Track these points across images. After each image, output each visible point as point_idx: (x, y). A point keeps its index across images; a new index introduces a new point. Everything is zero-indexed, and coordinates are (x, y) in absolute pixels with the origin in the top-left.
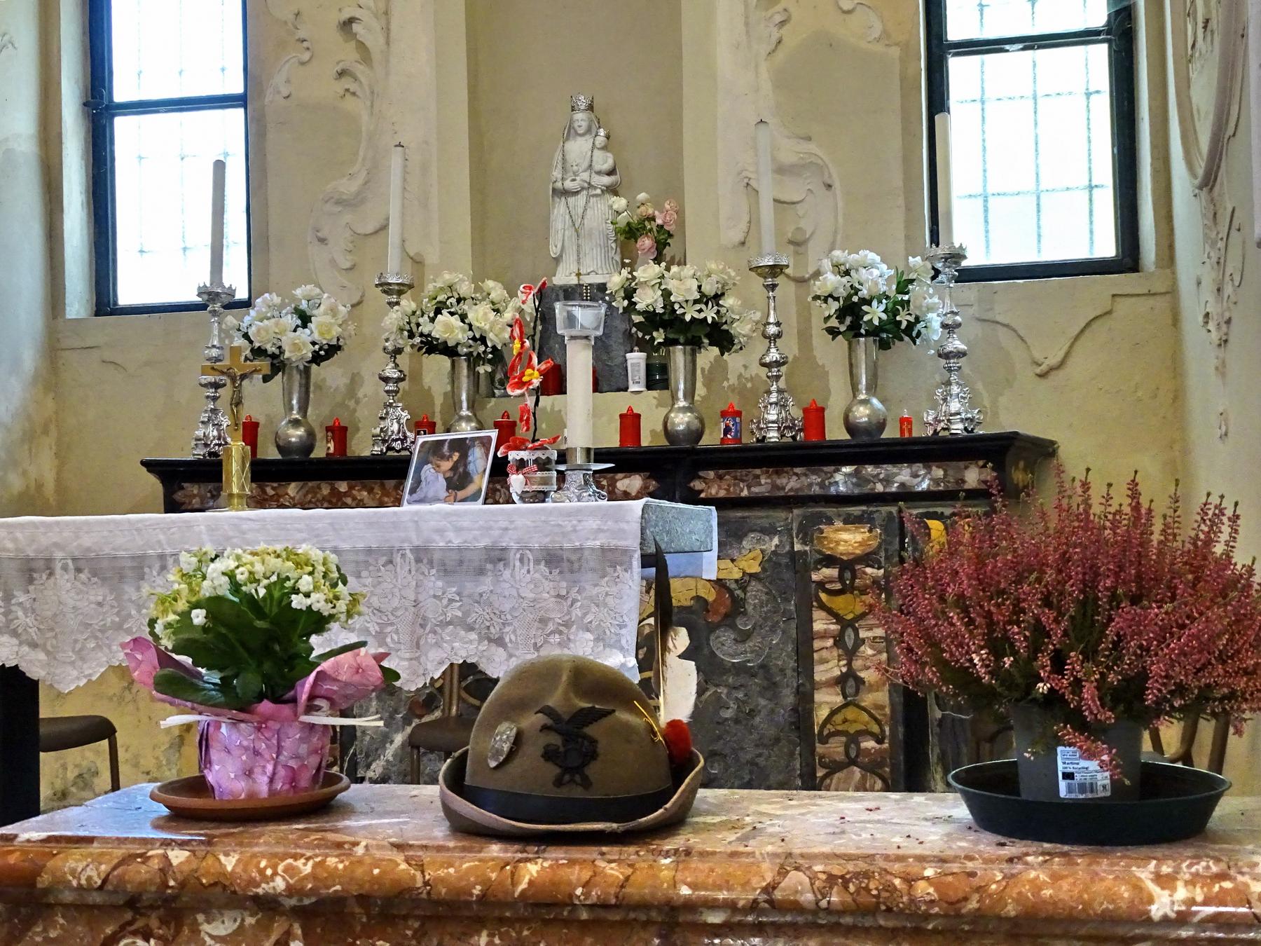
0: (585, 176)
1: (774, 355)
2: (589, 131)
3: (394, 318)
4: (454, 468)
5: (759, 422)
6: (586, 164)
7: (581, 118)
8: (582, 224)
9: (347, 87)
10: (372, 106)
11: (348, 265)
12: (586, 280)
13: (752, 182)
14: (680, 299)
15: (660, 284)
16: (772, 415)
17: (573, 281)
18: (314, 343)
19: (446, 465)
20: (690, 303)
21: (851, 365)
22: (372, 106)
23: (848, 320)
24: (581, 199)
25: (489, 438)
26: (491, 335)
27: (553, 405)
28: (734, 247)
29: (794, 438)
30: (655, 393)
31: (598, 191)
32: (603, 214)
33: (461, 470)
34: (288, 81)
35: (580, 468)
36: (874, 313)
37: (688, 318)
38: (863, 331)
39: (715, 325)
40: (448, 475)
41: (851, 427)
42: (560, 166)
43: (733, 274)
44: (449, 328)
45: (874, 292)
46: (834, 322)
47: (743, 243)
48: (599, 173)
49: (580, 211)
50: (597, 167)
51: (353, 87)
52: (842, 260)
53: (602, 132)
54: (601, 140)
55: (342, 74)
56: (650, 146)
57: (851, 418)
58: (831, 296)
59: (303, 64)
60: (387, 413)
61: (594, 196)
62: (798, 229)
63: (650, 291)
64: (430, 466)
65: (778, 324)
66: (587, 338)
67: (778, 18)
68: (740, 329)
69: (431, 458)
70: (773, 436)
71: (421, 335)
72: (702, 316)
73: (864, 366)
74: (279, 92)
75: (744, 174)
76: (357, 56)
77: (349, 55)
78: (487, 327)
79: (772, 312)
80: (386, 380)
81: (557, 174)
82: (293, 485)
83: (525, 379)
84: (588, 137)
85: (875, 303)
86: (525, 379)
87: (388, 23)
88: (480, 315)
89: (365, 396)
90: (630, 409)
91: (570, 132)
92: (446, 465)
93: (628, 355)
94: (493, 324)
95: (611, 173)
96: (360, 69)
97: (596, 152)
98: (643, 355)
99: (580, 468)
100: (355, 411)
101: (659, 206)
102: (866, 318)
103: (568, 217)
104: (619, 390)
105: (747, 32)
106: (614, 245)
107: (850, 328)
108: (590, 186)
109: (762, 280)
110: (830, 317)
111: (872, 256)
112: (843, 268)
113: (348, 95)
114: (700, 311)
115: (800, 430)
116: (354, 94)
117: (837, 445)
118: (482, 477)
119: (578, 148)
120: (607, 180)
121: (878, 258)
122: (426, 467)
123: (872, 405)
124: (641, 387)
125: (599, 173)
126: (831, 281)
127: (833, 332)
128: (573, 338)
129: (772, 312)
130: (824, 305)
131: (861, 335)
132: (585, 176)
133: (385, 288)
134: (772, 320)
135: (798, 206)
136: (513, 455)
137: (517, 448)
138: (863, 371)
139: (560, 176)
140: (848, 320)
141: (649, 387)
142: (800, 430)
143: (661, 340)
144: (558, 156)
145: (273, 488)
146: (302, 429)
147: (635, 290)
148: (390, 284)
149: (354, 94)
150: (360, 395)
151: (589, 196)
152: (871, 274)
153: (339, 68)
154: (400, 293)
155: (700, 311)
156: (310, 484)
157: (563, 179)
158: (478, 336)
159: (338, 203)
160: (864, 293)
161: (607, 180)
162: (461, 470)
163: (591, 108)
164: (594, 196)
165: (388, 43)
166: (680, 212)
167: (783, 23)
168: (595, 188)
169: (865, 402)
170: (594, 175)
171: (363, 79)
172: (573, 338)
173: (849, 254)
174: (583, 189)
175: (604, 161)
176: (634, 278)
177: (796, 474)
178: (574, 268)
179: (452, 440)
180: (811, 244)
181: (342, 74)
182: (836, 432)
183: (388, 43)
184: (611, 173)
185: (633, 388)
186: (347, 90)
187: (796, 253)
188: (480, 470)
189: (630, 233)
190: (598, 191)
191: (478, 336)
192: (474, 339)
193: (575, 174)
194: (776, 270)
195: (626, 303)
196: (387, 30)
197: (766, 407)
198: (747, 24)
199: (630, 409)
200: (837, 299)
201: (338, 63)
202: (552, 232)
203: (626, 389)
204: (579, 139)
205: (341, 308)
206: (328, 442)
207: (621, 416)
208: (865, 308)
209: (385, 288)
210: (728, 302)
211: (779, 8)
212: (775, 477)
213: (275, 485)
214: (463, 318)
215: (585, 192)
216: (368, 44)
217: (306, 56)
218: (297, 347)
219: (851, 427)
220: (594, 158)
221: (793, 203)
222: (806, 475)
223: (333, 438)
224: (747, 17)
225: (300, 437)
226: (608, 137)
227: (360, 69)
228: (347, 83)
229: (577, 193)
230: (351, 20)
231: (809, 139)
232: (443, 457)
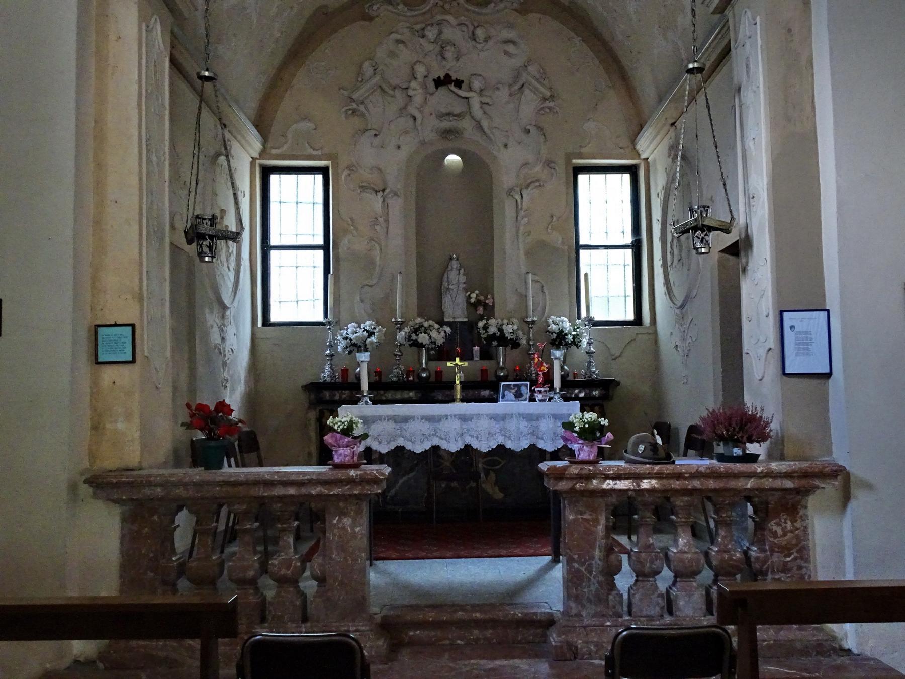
17: (452, 320)
80: (396, 355)
111: (565, 319)
124: (478, 359)
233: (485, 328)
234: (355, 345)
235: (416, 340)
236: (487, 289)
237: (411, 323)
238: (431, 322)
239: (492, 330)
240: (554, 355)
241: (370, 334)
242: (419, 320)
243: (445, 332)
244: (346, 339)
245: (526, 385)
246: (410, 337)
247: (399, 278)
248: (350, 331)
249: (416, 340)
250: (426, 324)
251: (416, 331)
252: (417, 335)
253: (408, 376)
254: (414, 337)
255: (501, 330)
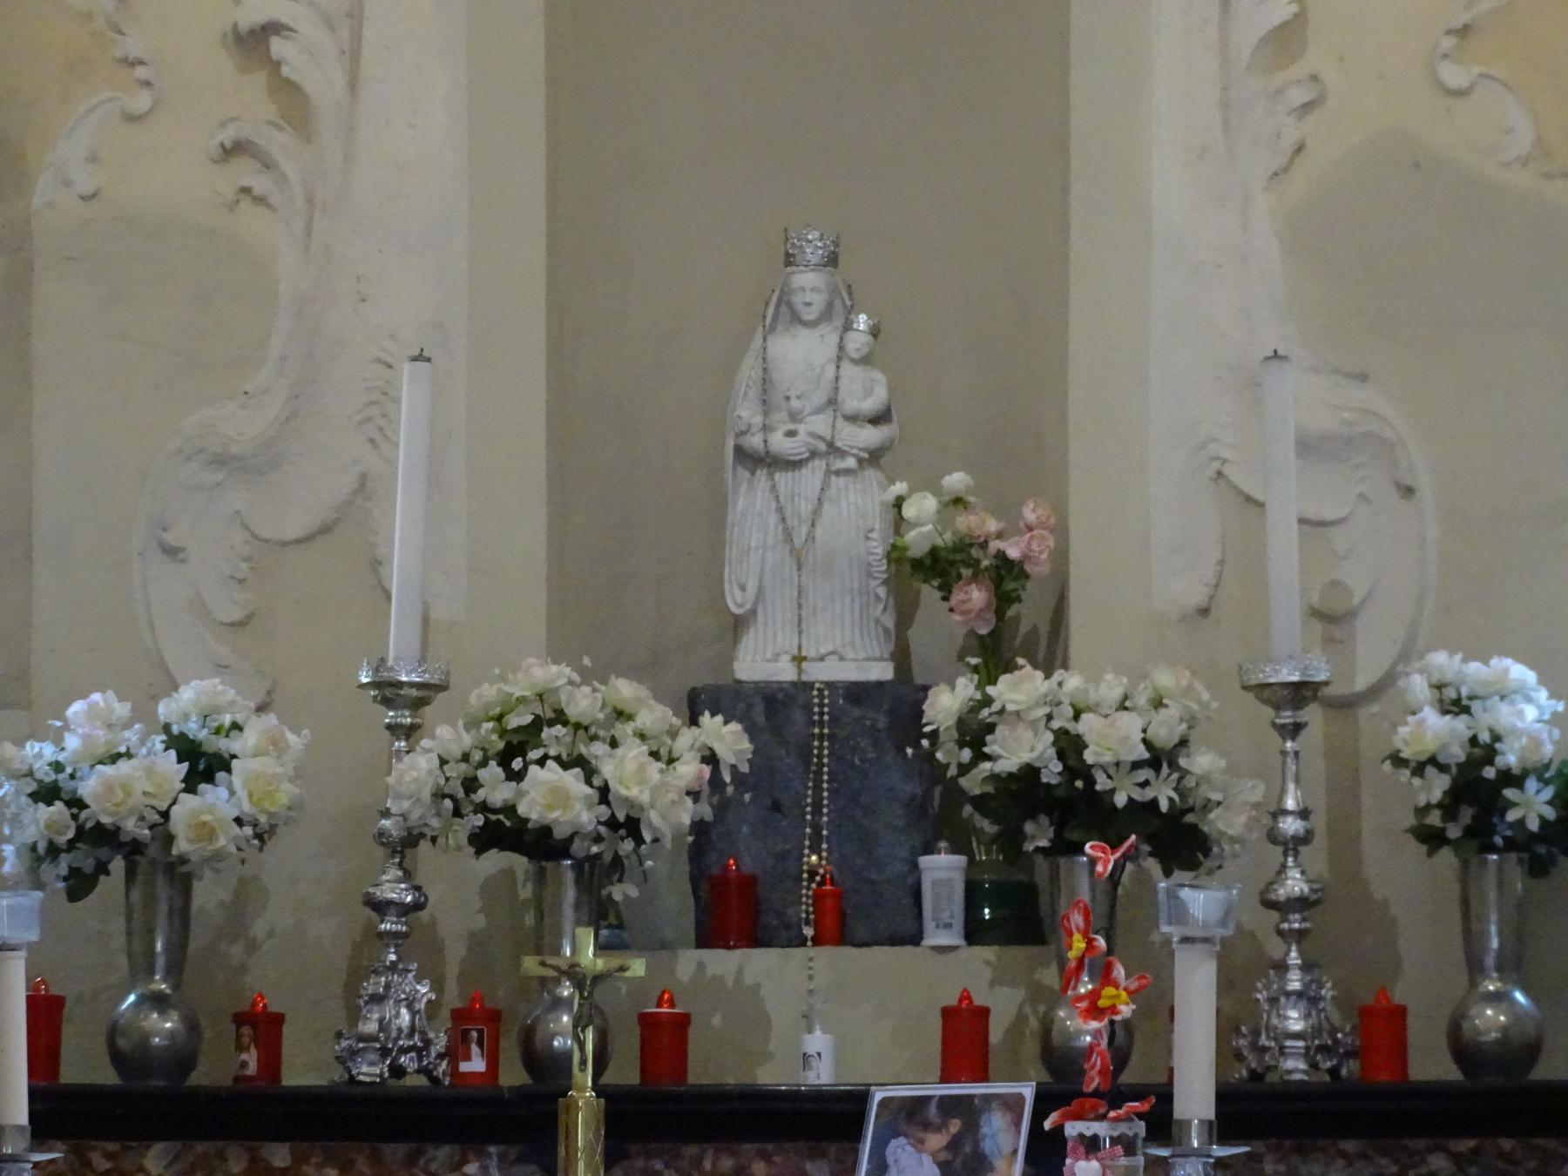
0: (821, 424)
1: (1295, 884)
2: (826, 315)
3: (417, 770)
4: (954, 1145)
5: (1256, 1033)
6: (820, 397)
7: (809, 284)
8: (811, 538)
9: (246, 182)
10: (309, 233)
11: (236, 614)
12: (819, 673)
13: (1226, 470)
14: (1108, 758)
15: (1049, 717)
16: (1295, 1020)
17: (785, 672)
18: (239, 821)
19: (937, 1141)
20: (1125, 768)
21: (1465, 903)
22: (309, 233)
23: (1467, 814)
24: (810, 478)
25: (1020, 1099)
26: (654, 817)
27: (740, 972)
28: (1183, 618)
29: (1334, 1072)
30: (988, 953)
31: (851, 462)
32: (853, 517)
33: (968, 1149)
34: (93, 158)
35: (1197, 1153)
36: (1528, 805)
37: (1120, 800)
38: (1498, 840)
39: (1177, 813)
40: (943, 1156)
41: (1462, 1049)
42: (753, 394)
43: (1205, 696)
44: (560, 797)
45: (1534, 759)
46: (1434, 819)
47: (1204, 612)
48: (852, 419)
49: (805, 508)
50: (851, 404)
51: (261, 184)
52: (1449, 676)
53: (862, 321)
54: (858, 340)
55: (235, 150)
56: (993, 372)
57: (1466, 1025)
58: (1433, 761)
59: (131, 118)
60: (387, 986)
61: (838, 473)
62: (1335, 584)
63: (1027, 735)
64: (902, 1140)
65: (1304, 814)
66: (1206, 940)
67: (1298, 96)
68: (1227, 823)
69: (903, 1127)
70: (1295, 1066)
71: (483, 808)
72: (1149, 794)
73: (1494, 917)
74: (68, 183)
75: (1213, 449)
76: (270, 111)
77: (247, 104)
78: (645, 798)
79: (1291, 787)
80: (380, 907)
81: (747, 411)
82: (158, 1148)
83: (1102, 1003)
84: (824, 329)
85: (1531, 784)
86: (1102, 1003)
87: (357, 37)
88: (627, 769)
89: (271, 934)
90: (966, 996)
91: (788, 314)
92: (937, 1141)
93: (925, 861)
94: (656, 789)
95: (878, 419)
96: (277, 143)
97: (848, 370)
98: (961, 860)
99: (1197, 1153)
100: (243, 968)
101: (1007, 510)
102: (1512, 816)
103: (773, 519)
104: (896, 941)
105: (1226, 124)
106: (882, 592)
107: (1469, 832)
108: (833, 450)
109: (1269, 712)
110: (1428, 807)
111: (1520, 673)
112: (1451, 693)
113: (246, 204)
114: (1145, 784)
115: (1350, 1054)
116: (261, 200)
117: (1433, 1092)
118: (1011, 1165)
119: (801, 354)
120: (870, 436)
121: (1530, 676)
122: (894, 1143)
123: (1513, 1001)
124: (953, 938)
125: (852, 419)
126: (1433, 730)
127: (1432, 839)
128: (1186, 940)
129: (1291, 787)
130: (1417, 781)
131: (1493, 848)
132: (821, 424)
133: (388, 692)
134: (1290, 804)
135: (1335, 532)
136: (1072, 1129)
137: (1078, 1117)
138: (1493, 929)
139: (758, 420)
140: (1467, 814)
141: (975, 933)
142: (1350, 1054)
143: (1044, 843)
144: (749, 370)
145: (109, 1156)
146: (175, 1015)
147: (991, 728)
148: (400, 685)
149: (261, 200)
150: (258, 929)
151: (829, 473)
152: (1521, 714)
153: (228, 135)
154: (418, 704)
155: (1145, 784)
156: (201, 1147)
157: (766, 428)
158: (621, 817)
159: (220, 461)
160: (1510, 758)
161: (870, 436)
162: (968, 1149)
163: (832, 260)
164: (838, 473)
165: (353, 86)
166: (1061, 531)
167: (1307, 107)
168: (842, 454)
169: (1497, 998)
170: (840, 422)
171: (289, 168)
172: (1186, 940)
173: (1465, 660)
174: (814, 454)
175: (866, 390)
176: (987, 701)
177: (1343, 1154)
178: (787, 641)
179: (942, 1098)
180: (1361, 623)
181: (235, 150)
182: (1431, 1063)
183: (353, 86)
184: (878, 419)
185: (935, 937)
186: (246, 190)
187: (1329, 641)
188: (1007, 1150)
189: (940, 567)
190: (851, 462)
191: (621, 817)
192: (612, 824)
193: (794, 417)
194: (1301, 693)
195: (966, 755)
196: (353, 55)
197: (1273, 1001)
198: (1225, 105)
199: (966, 996)
200: (1443, 768)
201: (223, 125)
202: (732, 552)
203: (915, 939)
204: (803, 333)
205: (292, 738)
206: (240, 1048)
207: (947, 1013)
208: (1509, 793)
209: (388, 692)
210: (1200, 761)
211: (1299, 70)
212: (1295, 1159)
213: (112, 1146)
214: (589, 772)
215: (819, 464)
216: (309, 87)
217: (142, 101)
218: (206, 832)
219: (1462, 1049)
220: (843, 383)
221: (1322, 524)
222: (1364, 1156)
223: (256, 1040)
224: (1225, 89)
225: (172, 1034)
226: (875, 332)
227: (277, 143)
228: (244, 172)
229: (794, 465)
230: (272, 28)
231: (1363, 377)
232: (927, 1126)
233: (975, 732)
234: (102, 837)
235: (510, 810)
236: (1025, 452)
237: (486, 693)
238: (625, 690)
239: (1016, 749)
240: (1180, 913)
241: (203, 765)
242: (557, 674)
243: (711, 758)
244: (46, 794)
245: (1012, 1105)
246: (471, 784)
247: (411, 385)
248: (72, 742)
249: (510, 810)
250: (582, 703)
251: (514, 751)
252: (517, 777)
253: (456, 1052)
254: (495, 788)
255: (1069, 746)
